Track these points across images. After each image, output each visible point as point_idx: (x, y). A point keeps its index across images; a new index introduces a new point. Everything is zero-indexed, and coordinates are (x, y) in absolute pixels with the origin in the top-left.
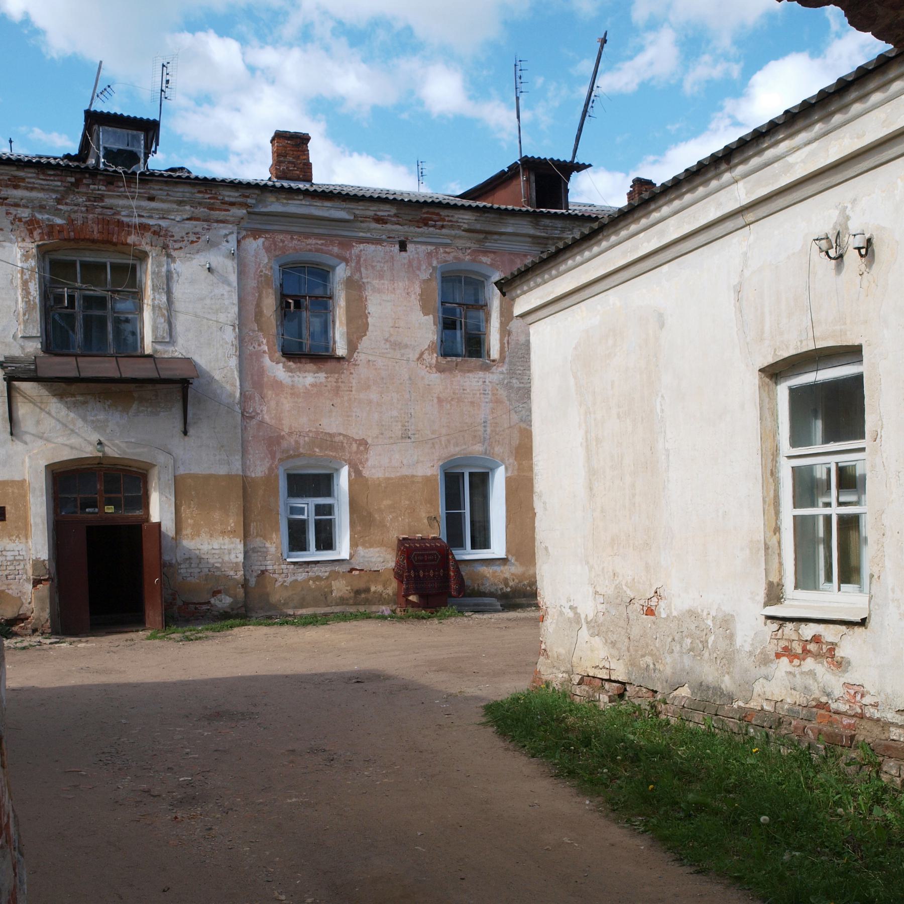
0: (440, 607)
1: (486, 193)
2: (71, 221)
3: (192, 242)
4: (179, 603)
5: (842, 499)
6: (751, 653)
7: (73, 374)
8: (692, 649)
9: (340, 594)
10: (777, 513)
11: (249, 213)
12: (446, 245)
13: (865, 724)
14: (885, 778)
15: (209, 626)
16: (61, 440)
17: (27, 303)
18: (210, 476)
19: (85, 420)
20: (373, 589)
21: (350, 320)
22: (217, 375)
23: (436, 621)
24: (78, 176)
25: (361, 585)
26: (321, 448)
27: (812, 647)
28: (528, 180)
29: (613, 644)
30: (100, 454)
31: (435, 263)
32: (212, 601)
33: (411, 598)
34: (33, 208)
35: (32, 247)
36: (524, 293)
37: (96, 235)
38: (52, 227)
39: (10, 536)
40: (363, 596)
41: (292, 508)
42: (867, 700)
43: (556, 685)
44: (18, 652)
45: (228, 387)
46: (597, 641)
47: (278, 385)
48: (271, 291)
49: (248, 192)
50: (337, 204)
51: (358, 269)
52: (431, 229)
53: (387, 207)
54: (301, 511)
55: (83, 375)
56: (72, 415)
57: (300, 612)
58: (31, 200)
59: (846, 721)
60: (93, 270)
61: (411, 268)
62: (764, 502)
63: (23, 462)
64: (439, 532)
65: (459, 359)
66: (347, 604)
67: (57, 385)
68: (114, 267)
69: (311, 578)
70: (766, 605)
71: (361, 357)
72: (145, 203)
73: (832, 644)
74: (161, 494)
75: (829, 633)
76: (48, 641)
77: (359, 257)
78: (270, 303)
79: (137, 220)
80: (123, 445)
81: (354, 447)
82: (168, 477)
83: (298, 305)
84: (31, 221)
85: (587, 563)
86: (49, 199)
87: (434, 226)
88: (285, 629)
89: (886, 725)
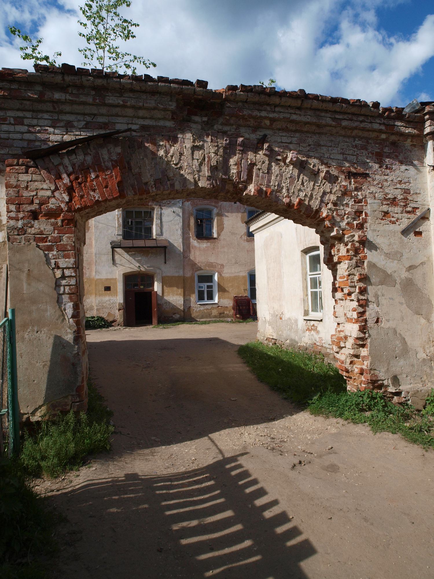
7: (131, 246)
8: (289, 329)
9: (214, 314)
10: (307, 290)
14: (325, 362)
15: (172, 324)
16: (127, 266)
17: (119, 224)
18: (173, 276)
19: (135, 259)
21: (218, 226)
22: (176, 245)
23: (245, 323)
25: (222, 311)
26: (208, 267)
27: (313, 328)
32: (173, 316)
40: (222, 315)
41: (199, 286)
42: (323, 342)
44: (113, 331)
45: (179, 248)
46: (270, 327)
51: (220, 210)
54: (202, 287)
56: (131, 258)
59: (319, 348)
60: (139, 213)
62: (303, 287)
63: (116, 273)
64: (247, 294)
68: (145, 212)
70: (304, 316)
71: (221, 237)
75: (315, 323)
77: (221, 206)
78: (192, 222)
81: (219, 266)
83: (201, 221)
88: (195, 325)
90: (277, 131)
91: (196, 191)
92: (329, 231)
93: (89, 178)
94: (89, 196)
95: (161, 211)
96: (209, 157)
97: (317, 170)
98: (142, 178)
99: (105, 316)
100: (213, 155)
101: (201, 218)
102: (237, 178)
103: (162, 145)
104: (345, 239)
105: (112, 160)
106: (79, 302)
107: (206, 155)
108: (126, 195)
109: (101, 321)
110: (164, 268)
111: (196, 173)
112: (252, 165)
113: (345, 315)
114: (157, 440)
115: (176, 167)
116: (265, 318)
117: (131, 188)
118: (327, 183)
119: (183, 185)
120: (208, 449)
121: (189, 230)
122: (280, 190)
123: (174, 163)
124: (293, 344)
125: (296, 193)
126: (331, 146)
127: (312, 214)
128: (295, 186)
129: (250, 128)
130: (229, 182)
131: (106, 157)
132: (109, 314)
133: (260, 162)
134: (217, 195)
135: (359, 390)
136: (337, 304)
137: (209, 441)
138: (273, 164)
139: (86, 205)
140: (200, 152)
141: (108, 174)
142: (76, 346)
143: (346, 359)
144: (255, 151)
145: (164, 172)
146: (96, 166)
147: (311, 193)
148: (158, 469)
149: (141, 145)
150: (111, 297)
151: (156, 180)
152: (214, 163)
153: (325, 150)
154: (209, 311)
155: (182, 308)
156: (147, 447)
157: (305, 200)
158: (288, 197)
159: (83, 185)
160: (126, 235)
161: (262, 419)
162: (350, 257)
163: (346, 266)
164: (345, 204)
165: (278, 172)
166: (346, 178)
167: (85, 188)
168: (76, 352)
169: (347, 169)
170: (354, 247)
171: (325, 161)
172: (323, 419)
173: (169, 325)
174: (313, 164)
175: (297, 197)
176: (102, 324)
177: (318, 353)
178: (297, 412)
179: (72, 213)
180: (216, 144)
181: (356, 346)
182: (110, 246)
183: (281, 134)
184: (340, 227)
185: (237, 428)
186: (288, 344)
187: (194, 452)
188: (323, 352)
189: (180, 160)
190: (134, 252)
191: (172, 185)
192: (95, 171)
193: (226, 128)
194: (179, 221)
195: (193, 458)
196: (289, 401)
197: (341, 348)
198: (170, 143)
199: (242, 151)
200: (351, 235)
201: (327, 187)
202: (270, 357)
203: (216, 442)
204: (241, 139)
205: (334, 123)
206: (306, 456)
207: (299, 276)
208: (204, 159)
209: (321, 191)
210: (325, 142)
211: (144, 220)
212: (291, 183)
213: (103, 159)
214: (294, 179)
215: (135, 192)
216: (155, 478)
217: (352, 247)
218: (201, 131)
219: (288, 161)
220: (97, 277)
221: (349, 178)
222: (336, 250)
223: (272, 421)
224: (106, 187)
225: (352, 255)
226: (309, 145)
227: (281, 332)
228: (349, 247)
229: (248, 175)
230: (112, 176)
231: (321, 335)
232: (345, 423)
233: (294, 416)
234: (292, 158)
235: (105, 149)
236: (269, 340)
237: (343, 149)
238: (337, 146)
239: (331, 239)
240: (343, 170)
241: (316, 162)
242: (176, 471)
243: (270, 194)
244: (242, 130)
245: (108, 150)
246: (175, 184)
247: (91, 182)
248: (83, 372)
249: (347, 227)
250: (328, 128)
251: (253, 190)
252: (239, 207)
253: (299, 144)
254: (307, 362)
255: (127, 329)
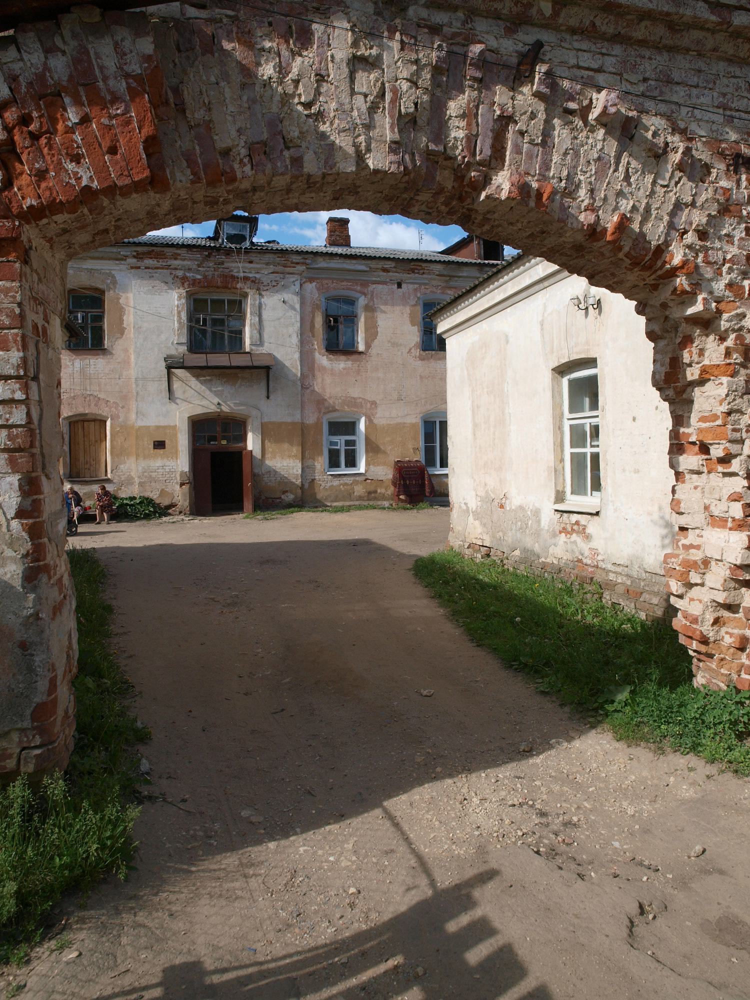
0: (419, 502)
1: (456, 250)
2: (205, 277)
3: (274, 286)
4: (263, 498)
5: (593, 444)
6: (548, 531)
7: (204, 364)
8: (521, 528)
10: (562, 451)
11: (307, 268)
12: (425, 284)
13: (599, 571)
14: (604, 601)
15: (280, 512)
16: (197, 402)
17: (179, 322)
19: (210, 390)
20: (379, 491)
22: (287, 363)
23: (415, 511)
24: (210, 251)
25: (372, 488)
26: (348, 406)
27: (575, 527)
28: (479, 243)
29: (485, 525)
30: (219, 410)
31: (419, 295)
32: (283, 497)
33: (401, 497)
34: (185, 270)
35: (183, 292)
36: (442, 321)
37: (219, 284)
38: (194, 280)
39: (168, 457)
40: (373, 495)
41: (331, 442)
42: (600, 558)
43: (456, 548)
44: (170, 524)
46: (477, 523)
47: (323, 369)
48: (320, 313)
49: (306, 256)
50: (359, 261)
52: (417, 275)
53: (390, 262)
54: (336, 444)
55: (209, 364)
57: (335, 504)
58: (183, 266)
61: (404, 300)
62: (554, 444)
64: (420, 457)
65: (434, 352)
66: (363, 500)
67: (195, 371)
68: (229, 301)
69: (341, 484)
70: (555, 503)
71: (373, 351)
72: (247, 265)
73: (584, 526)
74: (254, 433)
75: (583, 519)
76: (187, 519)
77: (373, 292)
78: (319, 321)
79: (242, 275)
80: (232, 405)
81: (369, 405)
82: (257, 423)
83: (336, 321)
84: (183, 277)
85: (473, 478)
86: (193, 265)
87: (418, 273)
88: (324, 514)
89: (608, 572)
90: (568, 37)
91: (358, 183)
92: (683, 303)
93: (61, 123)
94: (63, 174)
95: (260, 299)
96: (395, 91)
97: (662, 145)
98: (215, 137)
99: (154, 496)
100: (405, 86)
101: (336, 314)
102: (466, 153)
103: (270, 50)
104: (722, 323)
105: (127, 76)
106: (39, 472)
107: (387, 85)
108: (171, 182)
109: (148, 505)
110: (264, 405)
111: (361, 130)
112: (506, 120)
113: (706, 508)
114: (253, 819)
115: (306, 112)
116: (466, 504)
117: (185, 164)
118: (684, 180)
119: (326, 162)
120: (387, 853)
121: (313, 336)
122: (570, 192)
123: (303, 99)
124: (529, 558)
125: (612, 200)
126: (697, 86)
127: (647, 258)
128: (609, 183)
129: (501, 23)
130: (445, 163)
131: (110, 63)
132: (163, 493)
133: (525, 113)
134: (412, 199)
135: (732, 685)
136: (683, 482)
137: (388, 824)
138: (556, 122)
139: (55, 199)
140: (372, 76)
141: (117, 115)
142: (32, 596)
143: (704, 614)
144: (511, 84)
145: (275, 124)
146: (81, 89)
147: (647, 203)
148: (260, 934)
149: (211, 46)
150: (165, 460)
151: (253, 143)
152: (407, 106)
153: (682, 94)
154: (349, 487)
155: (299, 482)
156: (230, 846)
157: (630, 220)
158: (593, 210)
159: (43, 141)
160: (195, 345)
161: (502, 749)
162: (732, 368)
163: (723, 391)
164: (726, 235)
165: (568, 144)
166: (728, 170)
167: (50, 149)
168: (32, 611)
169: (731, 148)
170: (742, 344)
171: (682, 125)
172: (651, 755)
173: (275, 514)
174: (653, 128)
175: (614, 210)
176: (150, 511)
177: (588, 581)
178: (581, 733)
179: (13, 222)
180: (413, 56)
181: (733, 584)
182: (164, 364)
183: (577, 45)
184: (711, 293)
185: (449, 781)
186: (517, 559)
187: (353, 862)
188: (599, 577)
189: (318, 93)
190: (209, 376)
191: (297, 161)
192: (78, 102)
193: (440, 18)
194: (294, 318)
195: (352, 890)
196: (554, 699)
197: (690, 586)
198: (292, 46)
199: (480, 81)
200: (738, 315)
201: (686, 189)
202: (483, 586)
203: (406, 828)
204: (477, 49)
205: (713, 18)
206: (645, 879)
207: (545, 420)
208: (382, 95)
209: (670, 198)
210: (684, 75)
211: (229, 316)
212: (601, 174)
213: (101, 68)
214: (606, 164)
215: (194, 173)
216: (250, 978)
217: (736, 344)
218: (375, 17)
219: (593, 115)
220: (140, 423)
221: (736, 171)
222: (695, 351)
223: (528, 757)
224: (113, 151)
225: (737, 364)
226: (645, 80)
227: (501, 534)
228: (730, 342)
229: (493, 146)
230: (128, 122)
231: (594, 544)
232: (712, 769)
233: (577, 743)
234: (605, 107)
235: (108, 40)
236: (473, 548)
237: (724, 95)
238: (711, 86)
239: (684, 325)
240: (724, 150)
241: (660, 124)
242: (308, 942)
243: (548, 198)
244: (481, 25)
245: (116, 45)
246: (306, 158)
247: (66, 133)
248: (53, 665)
249: (727, 293)
250: (696, 34)
251: (506, 186)
252: (407, 295)
253: (621, 75)
254: (567, 599)
255: (197, 521)
